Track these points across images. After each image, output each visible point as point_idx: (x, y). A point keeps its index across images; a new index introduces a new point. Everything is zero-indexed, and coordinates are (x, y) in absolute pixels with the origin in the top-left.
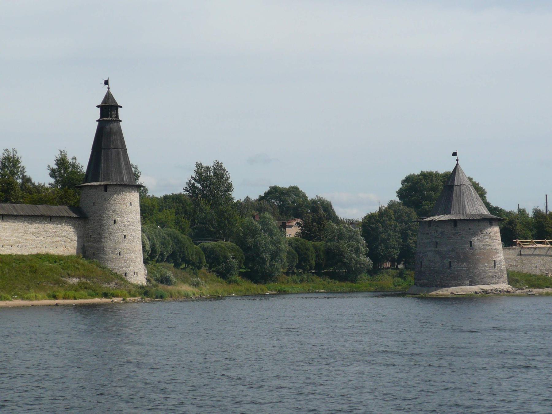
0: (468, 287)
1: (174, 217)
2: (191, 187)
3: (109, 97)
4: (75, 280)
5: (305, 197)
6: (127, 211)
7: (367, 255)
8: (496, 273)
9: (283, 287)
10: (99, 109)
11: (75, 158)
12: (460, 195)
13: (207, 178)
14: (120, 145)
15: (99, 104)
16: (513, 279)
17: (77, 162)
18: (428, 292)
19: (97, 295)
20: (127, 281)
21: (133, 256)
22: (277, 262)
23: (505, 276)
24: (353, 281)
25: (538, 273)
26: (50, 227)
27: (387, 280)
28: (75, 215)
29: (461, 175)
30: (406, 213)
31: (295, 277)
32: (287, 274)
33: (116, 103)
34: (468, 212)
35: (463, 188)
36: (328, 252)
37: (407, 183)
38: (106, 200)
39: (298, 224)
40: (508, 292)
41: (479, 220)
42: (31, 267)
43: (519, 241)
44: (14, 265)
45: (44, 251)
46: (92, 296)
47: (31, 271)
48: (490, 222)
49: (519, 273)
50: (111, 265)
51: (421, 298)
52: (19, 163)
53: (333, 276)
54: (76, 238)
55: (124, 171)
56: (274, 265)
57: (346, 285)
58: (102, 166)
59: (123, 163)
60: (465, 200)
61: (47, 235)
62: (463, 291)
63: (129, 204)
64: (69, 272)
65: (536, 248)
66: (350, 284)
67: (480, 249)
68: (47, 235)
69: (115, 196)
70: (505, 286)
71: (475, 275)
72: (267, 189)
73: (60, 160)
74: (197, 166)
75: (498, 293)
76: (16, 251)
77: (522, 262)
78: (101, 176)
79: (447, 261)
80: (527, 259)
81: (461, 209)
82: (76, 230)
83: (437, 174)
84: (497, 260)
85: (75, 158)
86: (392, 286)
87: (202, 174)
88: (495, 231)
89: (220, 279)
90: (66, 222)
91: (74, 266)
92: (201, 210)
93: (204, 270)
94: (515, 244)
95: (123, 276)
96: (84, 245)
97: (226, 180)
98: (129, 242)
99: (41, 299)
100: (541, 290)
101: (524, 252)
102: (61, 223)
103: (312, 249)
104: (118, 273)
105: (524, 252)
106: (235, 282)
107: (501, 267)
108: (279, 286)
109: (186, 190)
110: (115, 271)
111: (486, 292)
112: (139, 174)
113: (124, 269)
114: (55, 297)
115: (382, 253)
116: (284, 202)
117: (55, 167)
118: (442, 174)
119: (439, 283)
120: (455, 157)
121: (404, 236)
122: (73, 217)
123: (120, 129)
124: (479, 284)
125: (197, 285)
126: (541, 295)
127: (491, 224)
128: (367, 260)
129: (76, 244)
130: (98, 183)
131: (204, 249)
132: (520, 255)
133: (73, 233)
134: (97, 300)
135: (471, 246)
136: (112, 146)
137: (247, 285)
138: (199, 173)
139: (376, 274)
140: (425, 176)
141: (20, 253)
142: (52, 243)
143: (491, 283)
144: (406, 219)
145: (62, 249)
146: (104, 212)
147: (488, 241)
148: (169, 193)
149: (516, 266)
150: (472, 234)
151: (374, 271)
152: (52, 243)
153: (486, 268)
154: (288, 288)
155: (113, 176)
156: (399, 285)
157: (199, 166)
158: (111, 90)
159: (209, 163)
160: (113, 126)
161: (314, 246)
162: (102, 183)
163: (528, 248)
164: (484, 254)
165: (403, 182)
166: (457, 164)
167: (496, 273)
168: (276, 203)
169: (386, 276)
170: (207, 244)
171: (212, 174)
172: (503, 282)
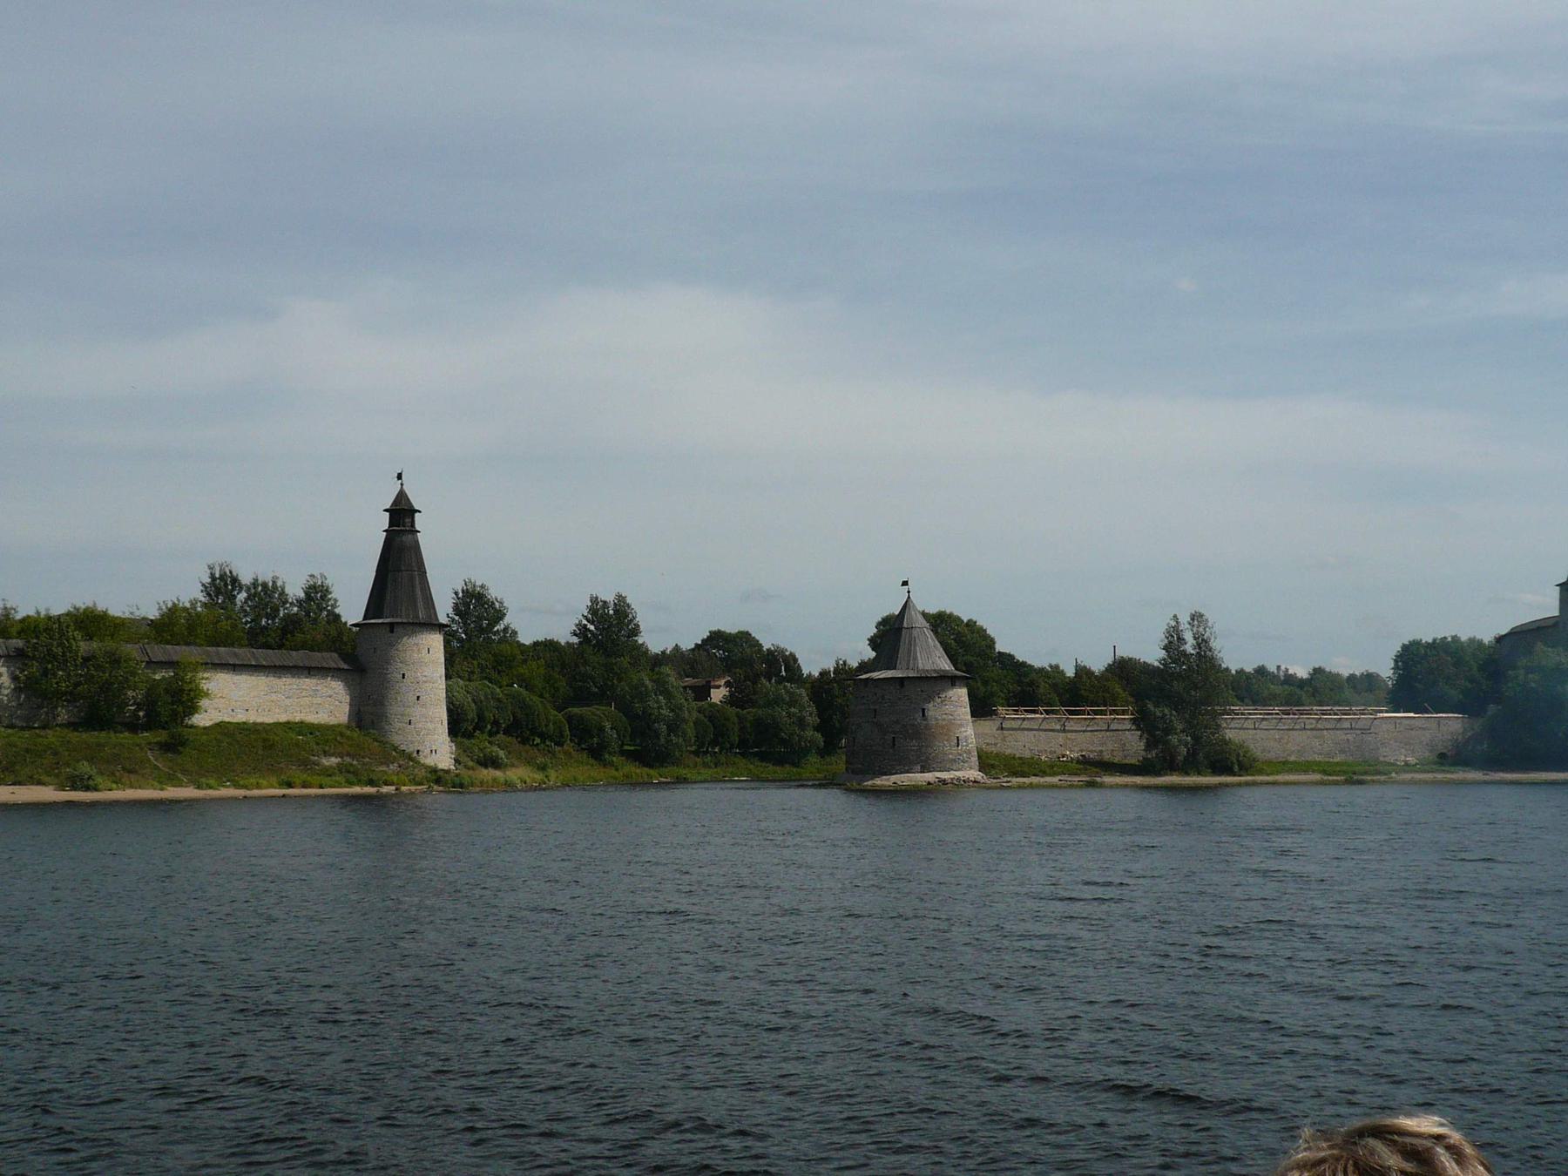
1: (542, 671)
2: (581, 631)
3: (402, 497)
4: (334, 760)
6: (425, 663)
7: (817, 729)
9: (683, 772)
16: (987, 763)
19: (360, 783)
21: (430, 726)
24: (794, 765)
25: (1027, 754)
26: (308, 683)
32: (696, 753)
35: (915, 632)
38: (391, 645)
39: (728, 684)
42: (265, 740)
44: (239, 737)
46: (350, 784)
47: (265, 748)
48: (953, 681)
50: (396, 739)
51: (849, 790)
53: (763, 757)
55: (420, 604)
57: (780, 772)
59: (418, 592)
70: (974, 774)
72: (706, 635)
76: (253, 718)
77: (1004, 739)
78: (386, 611)
79: (889, 737)
87: (597, 610)
88: (961, 694)
89: (592, 761)
92: (586, 663)
93: (568, 746)
94: (995, 713)
102: (325, 676)
106: (612, 764)
108: (683, 772)
109: (506, 629)
110: (403, 747)
111: (944, 782)
114: (290, 785)
116: (730, 653)
123: (417, 542)
125: (543, 768)
126: (1021, 787)
127: (953, 685)
128: (818, 735)
131: (570, 719)
134: (357, 790)
138: (593, 610)
139: (829, 754)
141: (259, 720)
148: (541, 639)
151: (828, 749)
153: (947, 748)
157: (594, 600)
159: (610, 598)
160: (407, 538)
161: (738, 715)
170: (576, 710)
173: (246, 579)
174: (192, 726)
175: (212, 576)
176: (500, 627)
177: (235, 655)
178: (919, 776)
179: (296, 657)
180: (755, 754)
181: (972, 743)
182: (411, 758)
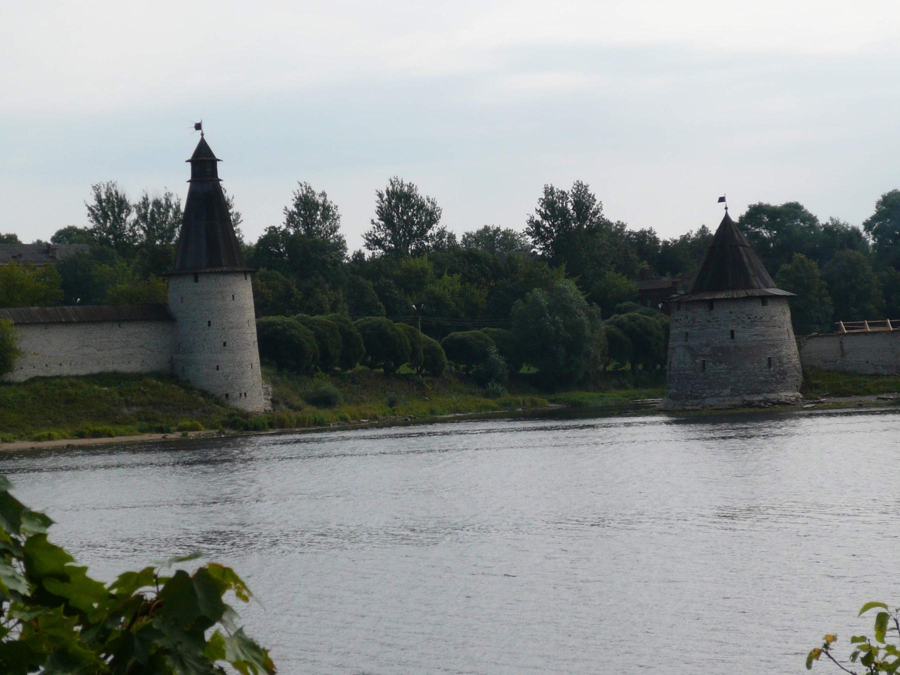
5: (812, 219)
8: (773, 376)
10: (189, 164)
17: (328, 199)
45: (110, 368)
52: (231, 207)
76: (66, 370)
85: (324, 194)
87: (552, 204)
91: (139, 390)
97: (595, 213)
99: (58, 439)
109: (441, 234)
120: (723, 204)
131: (620, 325)
157: (549, 192)
158: (205, 137)
159: (566, 185)
167: (773, 376)
173: (134, 198)
174: (9, 384)
175: (98, 198)
176: (433, 231)
182: (220, 401)
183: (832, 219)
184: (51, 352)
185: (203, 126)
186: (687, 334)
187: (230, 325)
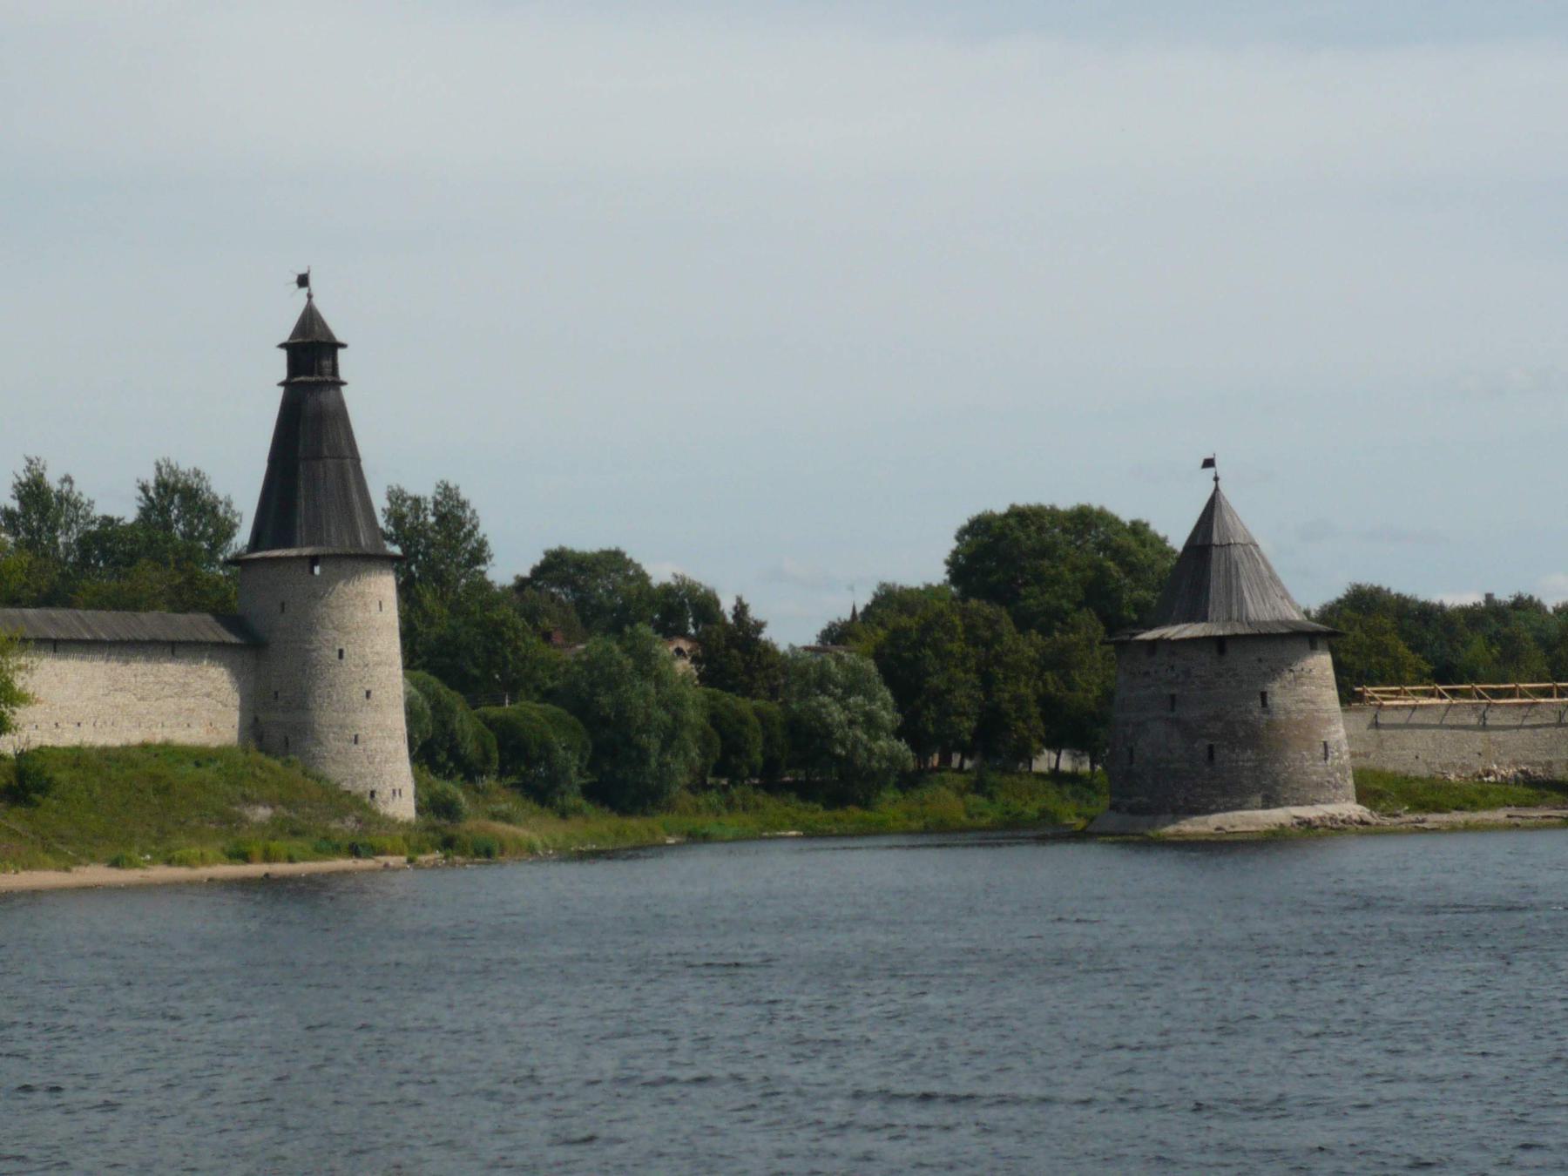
0: (1260, 813)
3: (310, 320)
5: (642, 577)
7: (898, 734)
8: (1330, 775)
10: (283, 353)
11: (68, 479)
12: (1228, 571)
13: (419, 531)
14: (347, 453)
15: (285, 338)
16: (1373, 788)
17: (76, 489)
18: (1151, 826)
19: (336, 851)
20: (376, 813)
22: (675, 755)
23: (1350, 782)
24: (866, 805)
25: (1423, 771)
26: (172, 670)
27: (945, 799)
28: (233, 639)
29: (1227, 518)
30: (986, 619)
31: (713, 797)
33: (330, 336)
34: (1252, 615)
36: (795, 726)
37: (974, 535)
38: (316, 596)
40: (1362, 822)
41: (1282, 636)
42: (155, 778)
43: (1370, 690)
47: (157, 791)
49: (1379, 775)
50: (334, 772)
54: (235, 699)
55: (361, 522)
56: (668, 765)
58: (302, 504)
60: (1244, 584)
61: (166, 692)
62: (1248, 824)
63: (374, 607)
64: (248, 791)
65: (1414, 708)
66: (856, 812)
67: (1288, 712)
68: (166, 692)
69: (340, 585)
70: (1351, 809)
71: (1276, 782)
72: (537, 559)
73: (27, 484)
74: (389, 499)
75: (1338, 829)
79: (1201, 746)
80: (1393, 736)
81: (1235, 608)
82: (238, 678)
83: (1053, 513)
84: (1331, 740)
85: (68, 479)
86: (963, 818)
88: (1321, 663)
90: (210, 657)
91: (254, 775)
95: (367, 799)
96: (256, 719)
97: (470, 534)
98: (378, 708)
100: (1445, 817)
101: (1385, 718)
102: (197, 659)
103: (753, 719)
104: (355, 792)
105: (1385, 718)
106: (577, 811)
107: (1340, 758)
110: (346, 786)
111: (1307, 824)
112: (237, 520)
113: (369, 779)
114: (245, 858)
115: (931, 729)
117: (15, 505)
118: (1065, 513)
119: (1181, 803)
120: (1210, 471)
121: (987, 682)
122: (231, 645)
123: (342, 403)
124: (1288, 804)
126: (1453, 829)
127: (1313, 648)
128: (902, 746)
129: (235, 717)
130: (293, 552)
132: (1376, 725)
133: (228, 686)
135: (1264, 704)
136: (326, 452)
137: (602, 825)
140: (1022, 517)
142: (178, 714)
143: (1318, 802)
144: (987, 634)
145: (202, 732)
146: (311, 629)
147: (1307, 690)
149: (1367, 755)
150: (1265, 674)
152: (178, 714)
154: (709, 824)
155: (333, 530)
156: (981, 814)
160: (326, 397)
162: (307, 551)
163: (1396, 708)
164: (1298, 725)
165: (959, 537)
166: (1217, 489)
167: (1330, 775)
168: (564, 595)
169: (942, 790)
171: (431, 519)
172: (1348, 799)
177: (54, 622)
178: (1262, 815)
179: (150, 623)
180: (789, 787)
181: (1342, 755)
183: (676, 576)
184: (82, 702)
185: (312, 281)
186: (1173, 697)
187: (376, 658)
